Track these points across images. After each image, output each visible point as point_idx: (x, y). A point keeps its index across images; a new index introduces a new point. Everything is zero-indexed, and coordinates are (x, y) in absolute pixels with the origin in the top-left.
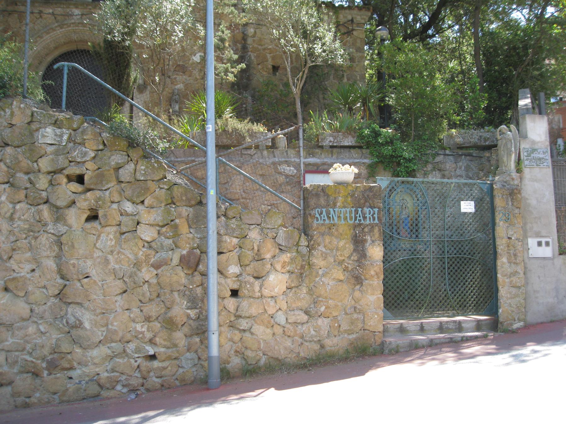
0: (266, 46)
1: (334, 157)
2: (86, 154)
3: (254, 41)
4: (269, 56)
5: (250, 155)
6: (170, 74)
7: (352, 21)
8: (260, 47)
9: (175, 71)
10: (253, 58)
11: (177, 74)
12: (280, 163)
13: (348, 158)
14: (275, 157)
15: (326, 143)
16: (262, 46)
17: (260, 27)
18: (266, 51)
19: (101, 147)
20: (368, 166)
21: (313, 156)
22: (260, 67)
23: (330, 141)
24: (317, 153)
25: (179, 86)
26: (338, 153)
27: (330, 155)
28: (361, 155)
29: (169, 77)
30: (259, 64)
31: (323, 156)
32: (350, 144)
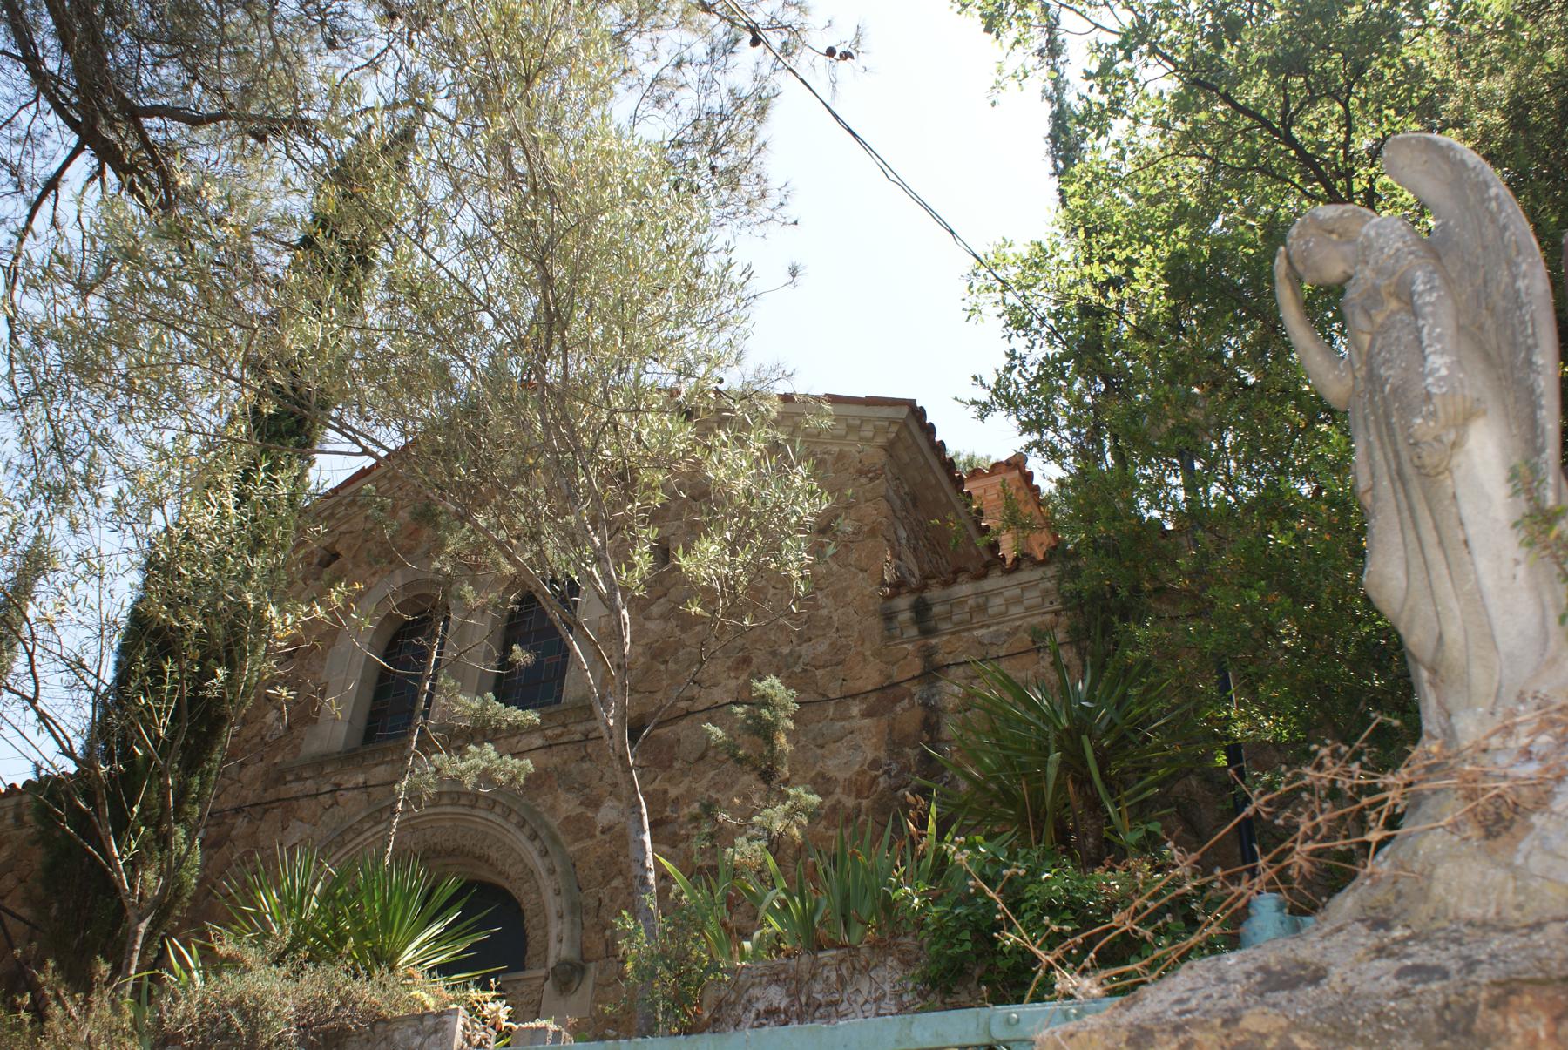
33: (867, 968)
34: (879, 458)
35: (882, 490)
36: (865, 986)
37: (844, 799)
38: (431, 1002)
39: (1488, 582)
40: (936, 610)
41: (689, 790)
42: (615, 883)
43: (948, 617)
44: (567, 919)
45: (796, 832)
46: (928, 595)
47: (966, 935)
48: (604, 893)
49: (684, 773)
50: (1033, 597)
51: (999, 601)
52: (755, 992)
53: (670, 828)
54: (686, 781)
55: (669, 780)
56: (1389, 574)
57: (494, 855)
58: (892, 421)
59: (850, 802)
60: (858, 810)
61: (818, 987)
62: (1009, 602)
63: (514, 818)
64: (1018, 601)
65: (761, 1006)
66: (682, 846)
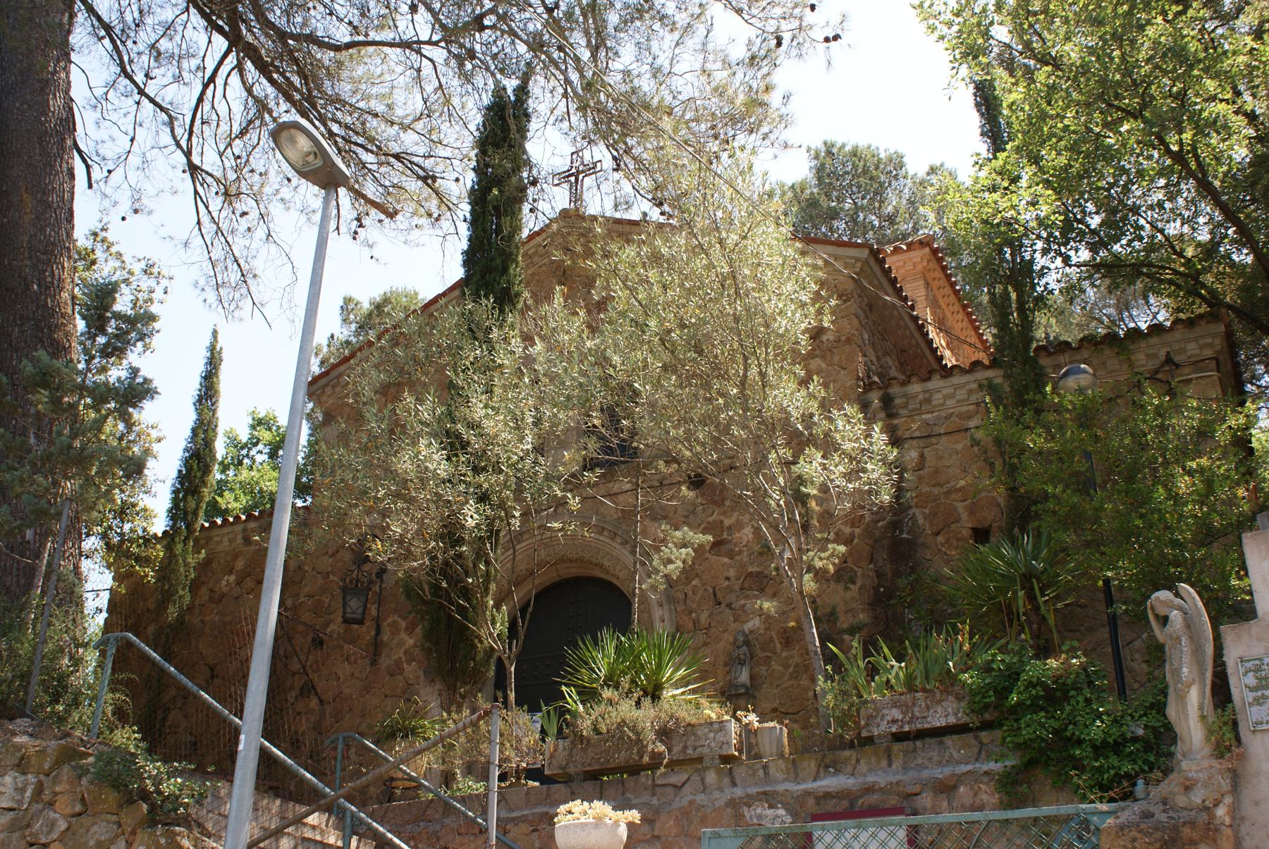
0: (952, 483)
1: (896, 765)
2: (52, 825)
3: (920, 478)
4: (960, 507)
5: (675, 786)
6: (732, 598)
7: (1169, 360)
8: (936, 491)
9: (742, 589)
10: (921, 521)
11: (747, 597)
12: (749, 801)
13: (939, 763)
14: (734, 784)
15: (881, 728)
16: (941, 486)
17: (934, 440)
18: (953, 496)
19: (78, 808)
20: (1000, 781)
21: (838, 772)
22: (940, 539)
23: (894, 721)
24: (848, 759)
25: (752, 622)
26: (906, 753)
27: (884, 763)
28: (976, 751)
29: (729, 606)
30: (938, 534)
31: (863, 766)
32: (952, 720)
33: (940, 701)
34: (850, 286)
35: (853, 310)
36: (940, 710)
37: (843, 528)
38: (713, 716)
39: (1192, 726)
40: (897, 401)
41: (737, 521)
42: (694, 583)
43: (905, 406)
44: (666, 607)
45: (831, 567)
46: (891, 391)
47: (991, 693)
48: (688, 590)
49: (733, 510)
50: (961, 395)
51: (939, 396)
52: (885, 711)
53: (728, 547)
54: (735, 514)
55: (724, 513)
56: (1172, 712)
57: (606, 563)
58: (857, 260)
59: (847, 530)
60: (852, 535)
61: (916, 709)
62: (946, 397)
63: (619, 540)
64: (952, 396)
65: (889, 718)
66: (737, 558)
